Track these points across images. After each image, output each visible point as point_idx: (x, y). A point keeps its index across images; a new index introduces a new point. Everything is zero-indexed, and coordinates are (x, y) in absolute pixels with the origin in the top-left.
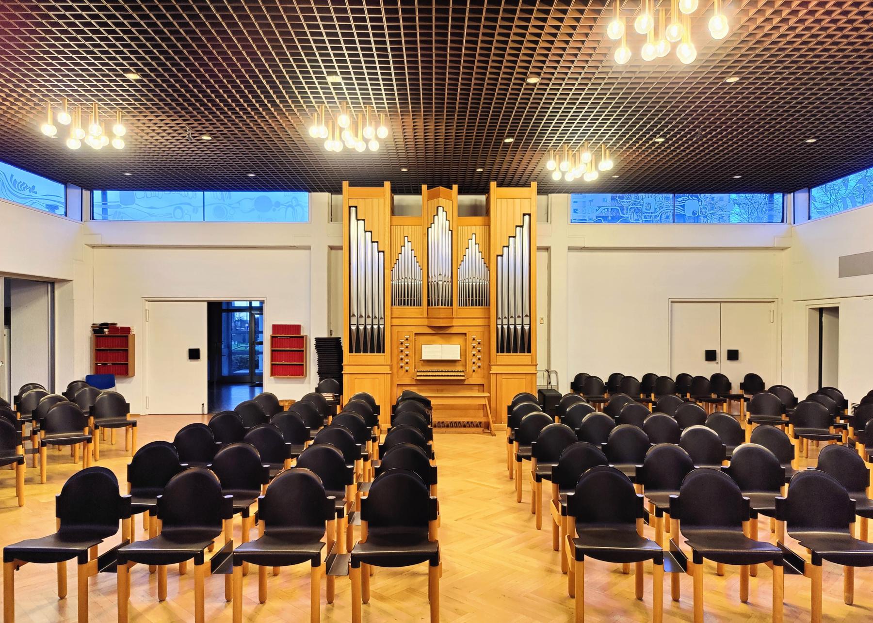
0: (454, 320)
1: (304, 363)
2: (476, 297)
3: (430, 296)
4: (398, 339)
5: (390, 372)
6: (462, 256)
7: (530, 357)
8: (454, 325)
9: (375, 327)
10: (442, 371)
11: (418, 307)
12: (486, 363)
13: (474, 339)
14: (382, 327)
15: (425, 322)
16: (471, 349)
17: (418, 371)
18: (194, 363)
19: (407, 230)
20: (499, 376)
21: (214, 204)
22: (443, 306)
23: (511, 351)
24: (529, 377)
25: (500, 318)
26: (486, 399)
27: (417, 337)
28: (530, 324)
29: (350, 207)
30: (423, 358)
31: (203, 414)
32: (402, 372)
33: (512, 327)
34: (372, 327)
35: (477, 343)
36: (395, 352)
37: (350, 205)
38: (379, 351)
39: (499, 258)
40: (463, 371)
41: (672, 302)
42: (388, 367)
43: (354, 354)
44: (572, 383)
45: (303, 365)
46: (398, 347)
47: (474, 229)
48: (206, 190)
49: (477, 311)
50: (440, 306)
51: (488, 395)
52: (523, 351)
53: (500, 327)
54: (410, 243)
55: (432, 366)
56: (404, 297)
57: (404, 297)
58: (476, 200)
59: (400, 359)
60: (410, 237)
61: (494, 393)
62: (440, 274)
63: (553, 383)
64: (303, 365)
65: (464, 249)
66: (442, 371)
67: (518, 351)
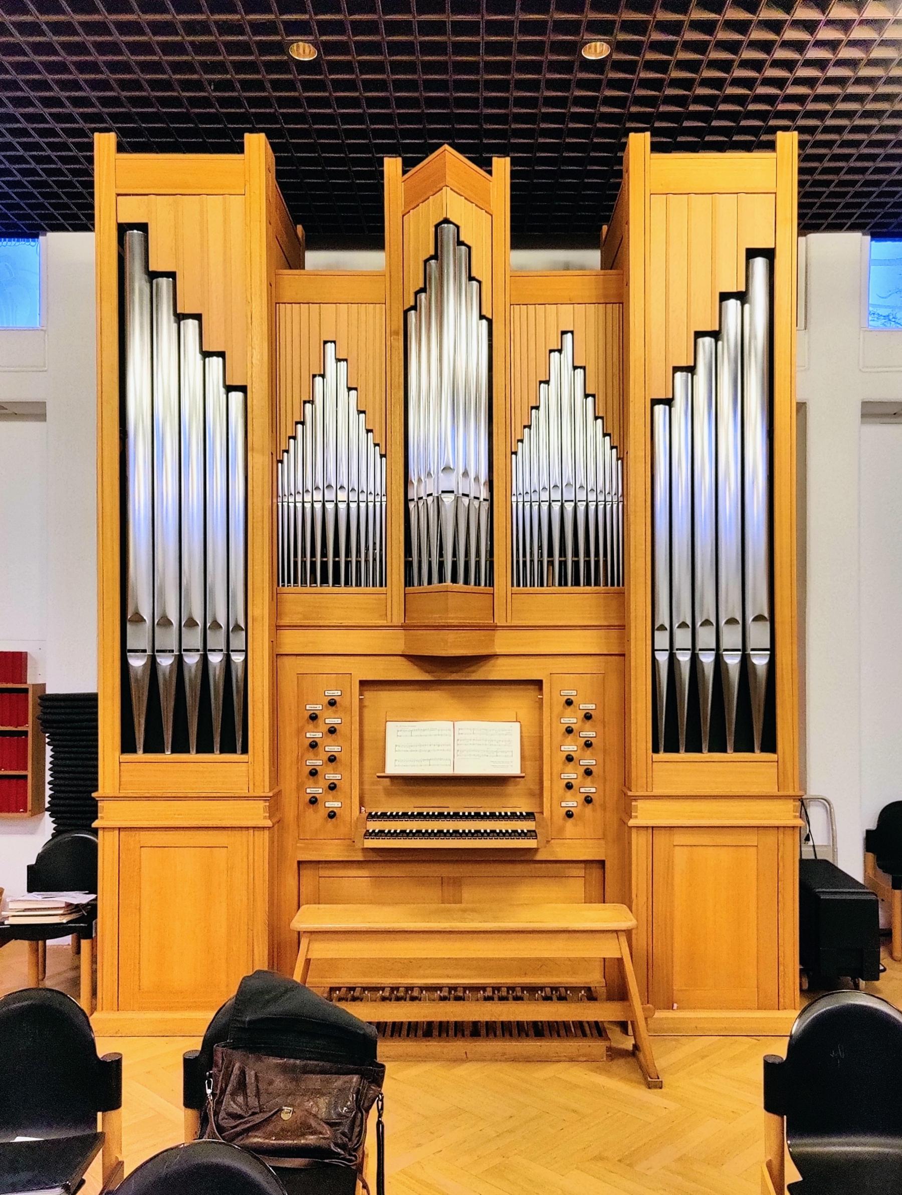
0: (499, 634)
1: (29, 773)
5: (269, 823)
6: (526, 409)
8: (498, 651)
9: (215, 659)
11: (371, 589)
12: (613, 785)
14: (237, 658)
15: (397, 642)
17: (371, 816)
20: (661, 839)
23: (705, 746)
25: (662, 628)
26: (623, 939)
27: (369, 695)
28: (772, 649)
29: (123, 229)
30: (392, 769)
32: (315, 818)
33: (707, 659)
34: (205, 660)
36: (290, 746)
37: (123, 220)
38: (228, 747)
40: (530, 816)
42: (262, 804)
43: (140, 755)
44: (868, 832)
45: (26, 777)
47: (567, 316)
52: (744, 745)
53: (663, 658)
56: (324, 554)
57: (324, 554)
59: (307, 770)
62: (447, 469)
63: (819, 837)
64: (26, 777)
65: (533, 384)
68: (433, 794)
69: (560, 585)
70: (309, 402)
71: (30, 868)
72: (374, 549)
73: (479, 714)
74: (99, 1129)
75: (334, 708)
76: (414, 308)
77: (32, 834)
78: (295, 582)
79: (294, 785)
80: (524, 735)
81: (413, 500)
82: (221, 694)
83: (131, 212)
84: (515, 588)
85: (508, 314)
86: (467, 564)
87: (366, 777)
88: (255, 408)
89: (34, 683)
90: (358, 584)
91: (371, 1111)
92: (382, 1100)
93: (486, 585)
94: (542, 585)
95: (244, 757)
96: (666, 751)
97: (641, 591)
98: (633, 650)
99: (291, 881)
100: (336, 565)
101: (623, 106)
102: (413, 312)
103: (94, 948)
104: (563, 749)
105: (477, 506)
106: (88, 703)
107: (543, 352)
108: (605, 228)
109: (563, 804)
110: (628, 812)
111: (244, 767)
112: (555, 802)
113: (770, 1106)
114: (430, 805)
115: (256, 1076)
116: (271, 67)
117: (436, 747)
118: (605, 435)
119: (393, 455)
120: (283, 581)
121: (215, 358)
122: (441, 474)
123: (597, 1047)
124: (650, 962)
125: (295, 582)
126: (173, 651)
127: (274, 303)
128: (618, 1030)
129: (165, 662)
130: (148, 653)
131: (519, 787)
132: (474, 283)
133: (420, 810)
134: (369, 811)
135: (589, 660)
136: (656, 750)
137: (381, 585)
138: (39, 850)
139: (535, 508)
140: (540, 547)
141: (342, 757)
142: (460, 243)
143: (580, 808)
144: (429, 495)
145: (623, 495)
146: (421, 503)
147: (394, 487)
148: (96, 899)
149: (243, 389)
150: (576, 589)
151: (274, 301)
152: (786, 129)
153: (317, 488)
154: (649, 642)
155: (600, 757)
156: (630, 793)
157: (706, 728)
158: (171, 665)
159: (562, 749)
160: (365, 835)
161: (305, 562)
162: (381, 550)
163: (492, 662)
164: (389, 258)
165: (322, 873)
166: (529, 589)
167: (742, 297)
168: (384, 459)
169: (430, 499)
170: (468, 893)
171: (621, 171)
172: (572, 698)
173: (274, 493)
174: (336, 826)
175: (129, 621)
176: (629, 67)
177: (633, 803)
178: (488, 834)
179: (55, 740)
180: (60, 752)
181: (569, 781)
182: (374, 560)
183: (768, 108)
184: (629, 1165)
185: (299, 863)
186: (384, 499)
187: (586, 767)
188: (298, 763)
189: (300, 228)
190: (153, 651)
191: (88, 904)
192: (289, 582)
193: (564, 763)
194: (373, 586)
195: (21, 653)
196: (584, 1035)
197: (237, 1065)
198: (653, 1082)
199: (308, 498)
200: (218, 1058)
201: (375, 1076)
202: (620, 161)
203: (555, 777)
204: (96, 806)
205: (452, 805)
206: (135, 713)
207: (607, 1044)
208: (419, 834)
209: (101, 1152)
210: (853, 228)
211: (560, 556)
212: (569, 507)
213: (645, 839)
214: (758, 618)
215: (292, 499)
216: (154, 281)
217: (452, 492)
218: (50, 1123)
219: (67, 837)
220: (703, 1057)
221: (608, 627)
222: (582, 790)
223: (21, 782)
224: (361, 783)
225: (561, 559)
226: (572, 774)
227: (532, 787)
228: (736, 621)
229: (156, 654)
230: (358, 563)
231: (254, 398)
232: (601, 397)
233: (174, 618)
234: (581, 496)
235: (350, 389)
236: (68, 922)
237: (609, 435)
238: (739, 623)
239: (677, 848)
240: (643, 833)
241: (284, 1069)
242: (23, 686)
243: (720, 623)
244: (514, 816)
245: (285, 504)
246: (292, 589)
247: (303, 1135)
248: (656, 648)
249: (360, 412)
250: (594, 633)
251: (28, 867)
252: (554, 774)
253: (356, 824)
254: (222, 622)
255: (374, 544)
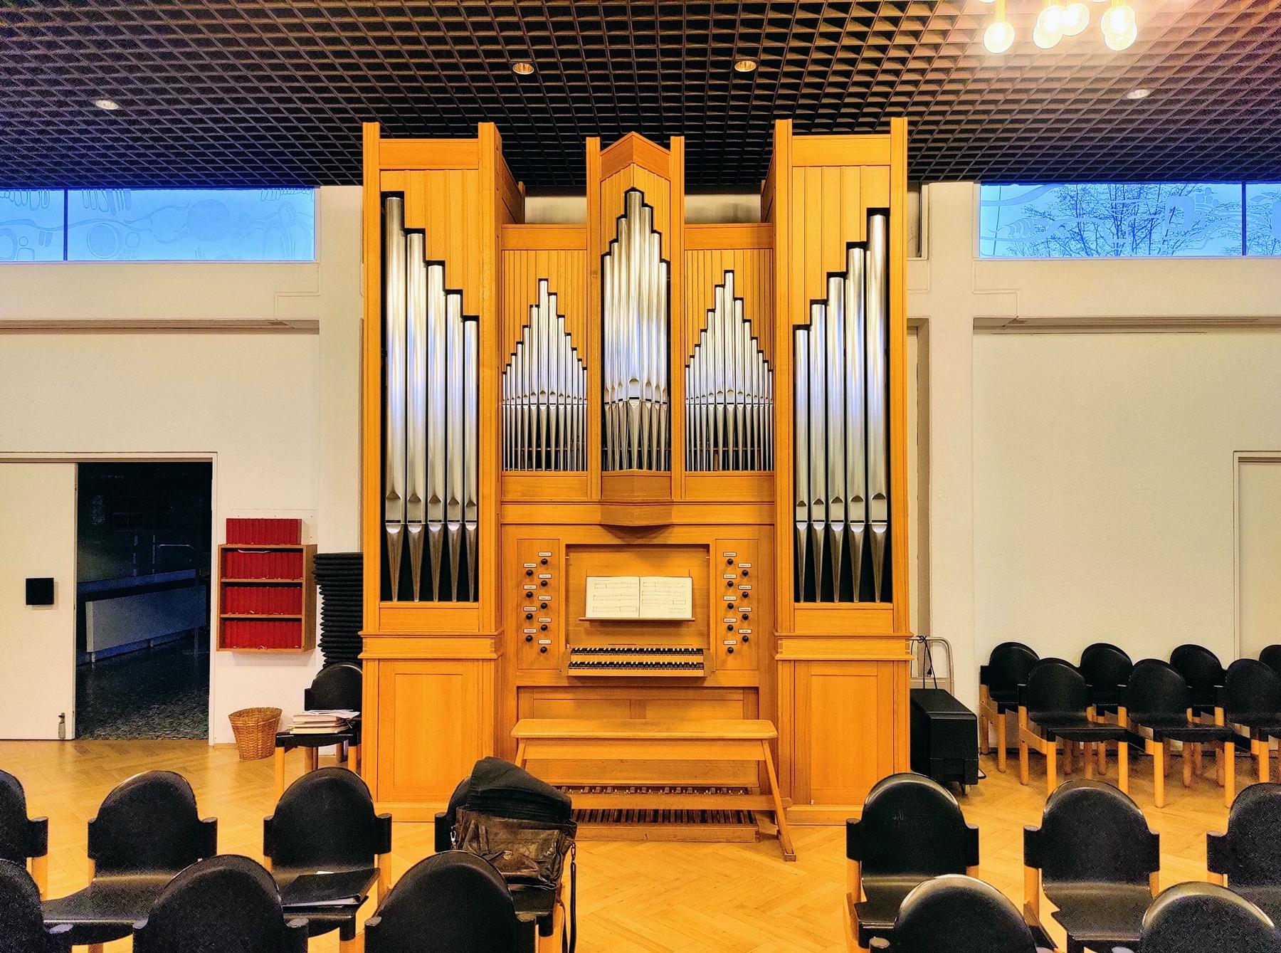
0: (675, 508)
1: (303, 617)
3: (609, 444)
4: (520, 561)
5: (494, 656)
7: (888, 616)
8: (675, 521)
9: (454, 528)
10: (641, 651)
11: (575, 472)
14: (471, 527)
15: (595, 514)
17: (574, 651)
18: (41, 612)
19: (547, 262)
20: (801, 670)
21: (88, 222)
22: (625, 470)
23: (836, 596)
24: (887, 670)
25: (802, 504)
26: (767, 746)
27: (573, 555)
29: (385, 196)
30: (591, 614)
31: (63, 740)
32: (530, 653)
34: (445, 528)
35: (740, 572)
36: (512, 597)
38: (463, 597)
39: (801, 334)
40: (700, 651)
41: (1242, 460)
42: (489, 642)
43: (395, 602)
44: (983, 668)
45: (300, 620)
46: (519, 585)
47: (729, 259)
48: (78, 186)
49: (738, 484)
51: (771, 733)
52: (868, 596)
53: (802, 527)
54: (553, 298)
55: (613, 634)
56: (539, 445)
57: (539, 445)
58: (736, 207)
59: (524, 615)
60: (553, 280)
61: (786, 719)
62: (634, 380)
63: (940, 670)
66: (641, 651)
68: (626, 634)
69: (724, 469)
70: (527, 326)
71: (306, 691)
72: (578, 441)
73: (659, 571)
74: (376, 866)
76: (609, 253)
77: (305, 666)
78: (516, 467)
79: (514, 627)
82: (458, 551)
83: (391, 182)
84: (688, 472)
85: (682, 258)
86: (650, 452)
89: (307, 544)
91: (567, 855)
92: (575, 848)
94: (709, 470)
95: (475, 605)
96: (805, 601)
98: (779, 521)
99: (511, 702)
100: (548, 453)
101: (770, 101)
102: (608, 257)
103: (359, 753)
106: (353, 562)
107: (709, 288)
109: (726, 642)
110: (775, 648)
112: (719, 641)
113: (851, 855)
114: (622, 642)
115: (486, 830)
116: (499, 78)
117: (626, 597)
118: (759, 352)
120: (506, 466)
121: (455, 295)
123: (747, 831)
124: (793, 763)
125: (516, 467)
127: (501, 250)
128: (767, 820)
129: (415, 530)
132: (656, 235)
133: (613, 647)
134: (572, 647)
136: (797, 599)
138: (314, 677)
140: (708, 440)
142: (644, 205)
145: (773, 399)
148: (360, 716)
149: (476, 318)
150: (736, 472)
152: (898, 115)
153: (533, 394)
154: (792, 515)
155: (755, 605)
157: (837, 584)
158: (420, 532)
161: (524, 451)
162: (583, 442)
164: (590, 204)
165: (536, 696)
167: (865, 246)
169: (621, 404)
170: (651, 713)
171: (772, 143)
173: (500, 398)
174: (547, 659)
176: (773, 76)
178: (666, 666)
179: (326, 590)
180: (329, 600)
182: (578, 449)
183: (879, 110)
184: (763, 911)
185: (518, 688)
186: (585, 402)
189: (521, 183)
190: (406, 521)
191: (352, 720)
192: (511, 467)
193: (726, 611)
195: (296, 520)
196: (740, 822)
197: (473, 822)
198: (790, 857)
199: (526, 401)
200: (459, 817)
201: (571, 833)
202: (771, 136)
203: (719, 620)
204: (361, 642)
205: (639, 643)
206: (392, 570)
207: (756, 828)
209: (376, 884)
210: (965, 178)
211: (724, 446)
212: (731, 408)
217: (638, 398)
218: (340, 862)
219: (337, 667)
220: (831, 840)
222: (741, 631)
223: (296, 623)
226: (732, 619)
232: (755, 323)
233: (421, 495)
234: (740, 399)
235: (559, 316)
236: (338, 733)
237: (762, 352)
240: (787, 664)
241: (506, 825)
242: (298, 547)
244: (687, 652)
245: (508, 406)
246: (513, 472)
247: (519, 869)
251: (306, 690)
255: (578, 437)
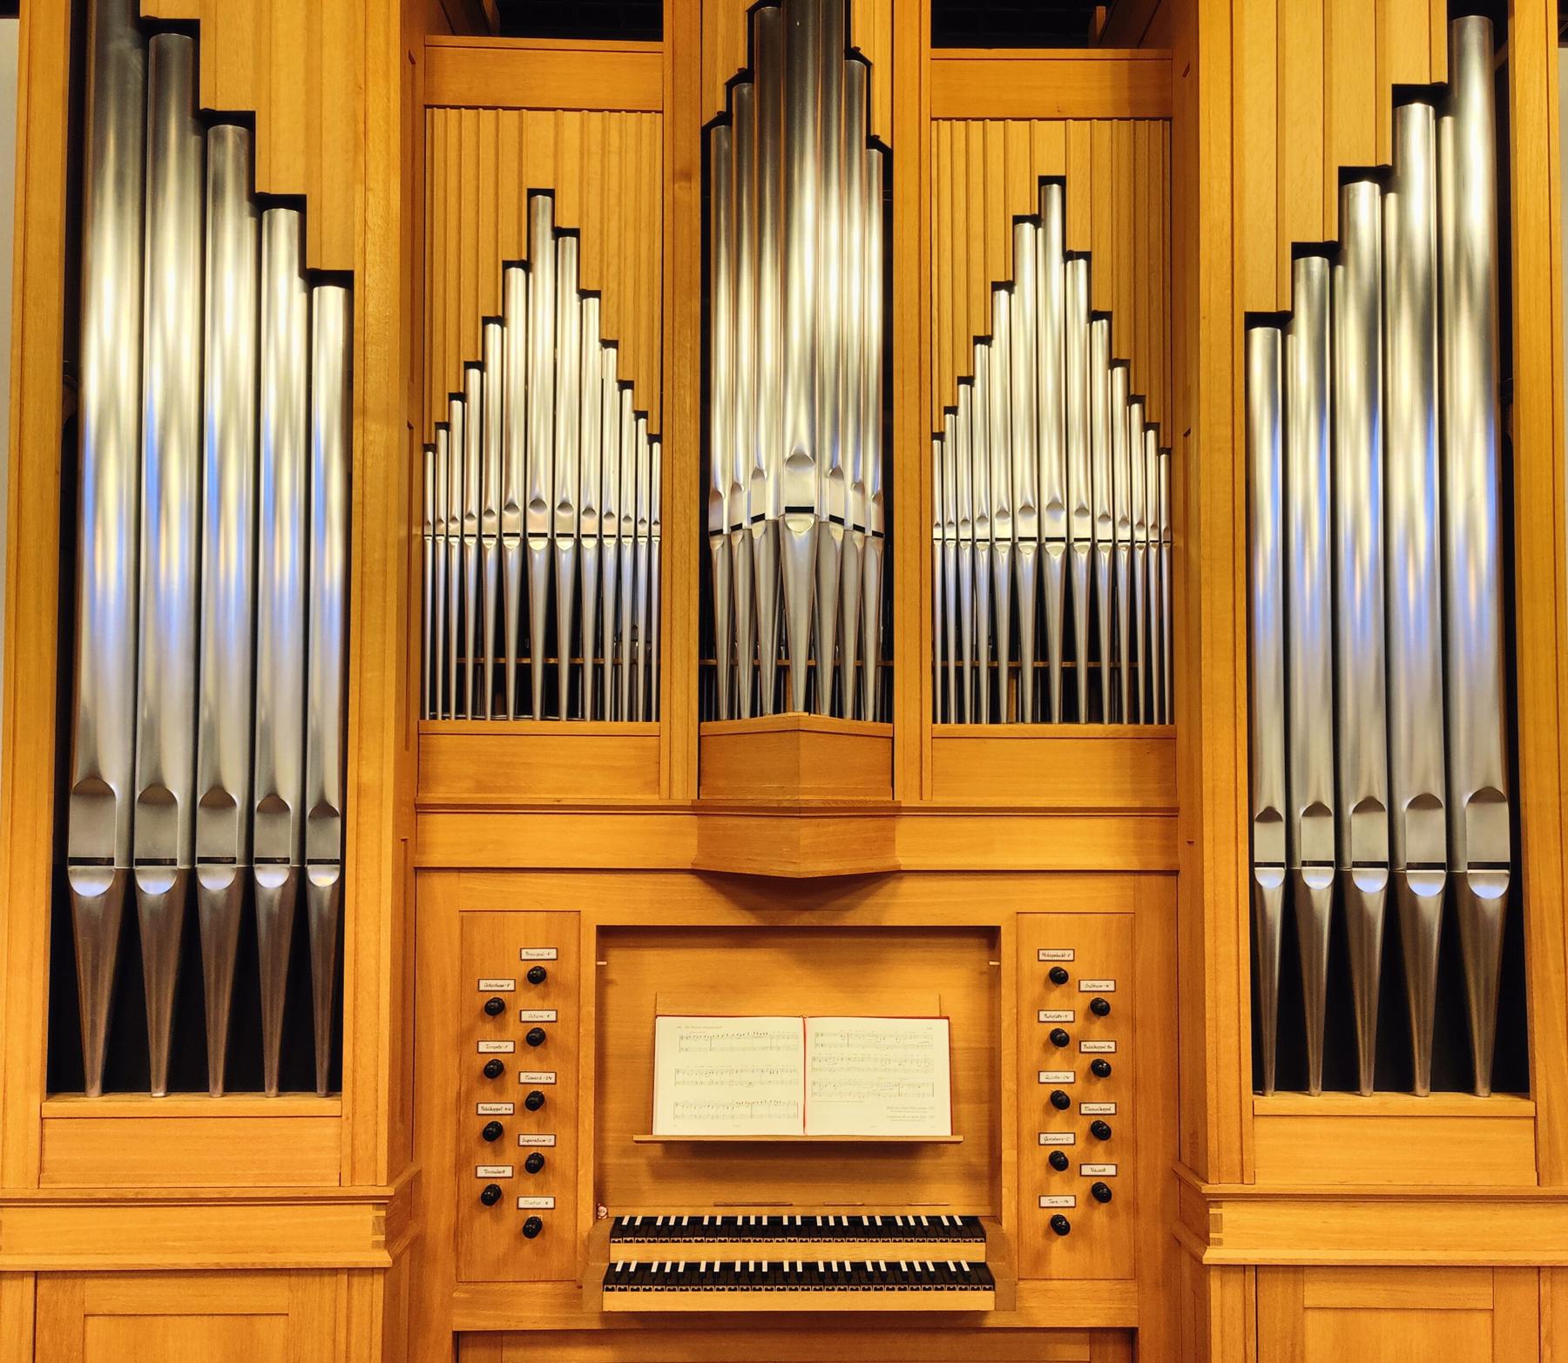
2: (1069, 651)
4: (467, 973)
5: (383, 1258)
8: (905, 861)
11: (624, 726)
12: (1156, 1157)
13: (1058, 977)
14: (323, 879)
16: (1034, 1052)
17: (622, 1231)
20: (1276, 1293)
25: (1270, 815)
27: (618, 957)
28: (1516, 868)
30: (671, 1122)
38: (297, 1079)
40: (971, 1228)
43: (94, 1101)
50: (824, 717)
53: (1272, 882)
56: (524, 649)
57: (524, 649)
59: (478, 1126)
67: (1366, 1073)
72: (634, 640)
75: (541, 986)
78: (461, 709)
79: (449, 1160)
80: (955, 1045)
81: (720, 532)
86: (838, 671)
87: (612, 1139)
88: (370, 320)
90: (598, 715)
93: (875, 720)
97: (1225, 733)
100: (551, 673)
104: (1043, 1077)
105: (860, 546)
108: (1101, 11)
109: (1045, 1202)
111: (330, 1129)
112: (1027, 1196)
119: (677, 438)
120: (433, 707)
122: (785, 471)
125: (461, 709)
126: (173, 862)
130: (116, 867)
131: (945, 1160)
135: (1101, 883)
136: (1259, 1086)
137: (648, 718)
139: (983, 557)
141: (560, 1097)
143: (1081, 1209)
144: (756, 519)
146: (738, 537)
147: (679, 506)
149: (344, 279)
151: (420, 101)
154: (1244, 847)
155: (1125, 1094)
156: (1206, 1189)
159: (1043, 1079)
160: (606, 1282)
162: (648, 642)
163: (891, 886)
166: (968, 727)
168: (656, 446)
169: (758, 529)
172: (1063, 966)
175: (75, 794)
177: (1212, 1211)
181: (1058, 1149)
182: (633, 663)
185: (457, 1335)
186: (656, 529)
187: (1094, 1119)
188: (458, 1108)
192: (446, 708)
193: (1047, 1112)
194: (631, 719)
203: (1026, 1141)
205: (797, 1202)
208: (729, 1277)
213: (1238, 1292)
214: (1483, 796)
215: (454, 527)
216: (152, 41)
217: (809, 510)
221: (1143, 812)
222: (1086, 1170)
224: (600, 1149)
225: (1036, 664)
226: (1063, 1135)
227: (973, 1160)
228: (1378, 806)
229: (198, 866)
230: (598, 669)
231: (369, 299)
232: (1122, 319)
238: (1384, 810)
239: (1310, 1313)
240: (1235, 1279)
243: (1456, 802)
244: (935, 1230)
246: (453, 724)
248: (1256, 860)
249: (606, 344)
250: (1111, 824)
252: (1025, 1133)
253: (587, 1248)
254: (289, 796)
255: (634, 628)
